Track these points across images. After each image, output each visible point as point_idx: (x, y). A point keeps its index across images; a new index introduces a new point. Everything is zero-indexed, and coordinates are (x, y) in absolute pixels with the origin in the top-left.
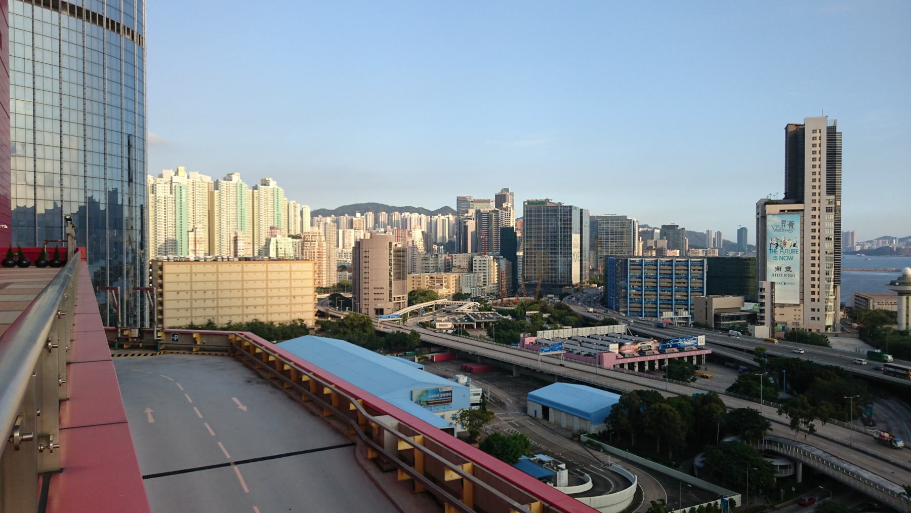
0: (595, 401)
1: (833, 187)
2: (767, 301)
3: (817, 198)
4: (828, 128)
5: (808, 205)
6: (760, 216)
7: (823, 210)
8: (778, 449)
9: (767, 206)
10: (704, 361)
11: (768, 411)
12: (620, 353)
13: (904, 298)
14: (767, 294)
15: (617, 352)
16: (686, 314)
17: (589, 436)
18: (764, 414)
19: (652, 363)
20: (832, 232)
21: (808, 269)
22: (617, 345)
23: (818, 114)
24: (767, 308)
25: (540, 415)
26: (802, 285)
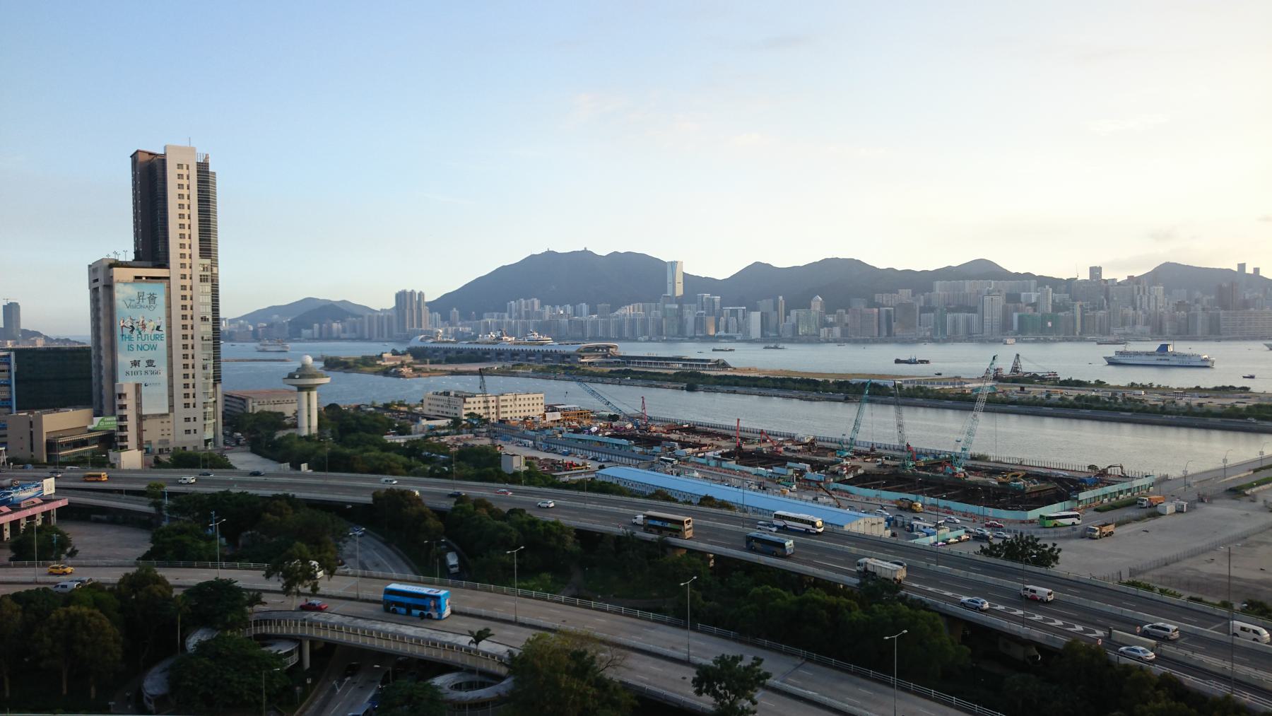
1: (207, 249)
2: (130, 413)
3: (187, 261)
4: (199, 164)
5: (174, 270)
6: (100, 285)
7: (196, 278)
8: (271, 630)
9: (115, 269)
10: (54, 521)
11: (247, 578)
13: (305, 393)
14: (130, 401)
18: (240, 584)
20: (209, 309)
21: (178, 362)
23: (184, 143)
24: (131, 423)
26: (171, 386)
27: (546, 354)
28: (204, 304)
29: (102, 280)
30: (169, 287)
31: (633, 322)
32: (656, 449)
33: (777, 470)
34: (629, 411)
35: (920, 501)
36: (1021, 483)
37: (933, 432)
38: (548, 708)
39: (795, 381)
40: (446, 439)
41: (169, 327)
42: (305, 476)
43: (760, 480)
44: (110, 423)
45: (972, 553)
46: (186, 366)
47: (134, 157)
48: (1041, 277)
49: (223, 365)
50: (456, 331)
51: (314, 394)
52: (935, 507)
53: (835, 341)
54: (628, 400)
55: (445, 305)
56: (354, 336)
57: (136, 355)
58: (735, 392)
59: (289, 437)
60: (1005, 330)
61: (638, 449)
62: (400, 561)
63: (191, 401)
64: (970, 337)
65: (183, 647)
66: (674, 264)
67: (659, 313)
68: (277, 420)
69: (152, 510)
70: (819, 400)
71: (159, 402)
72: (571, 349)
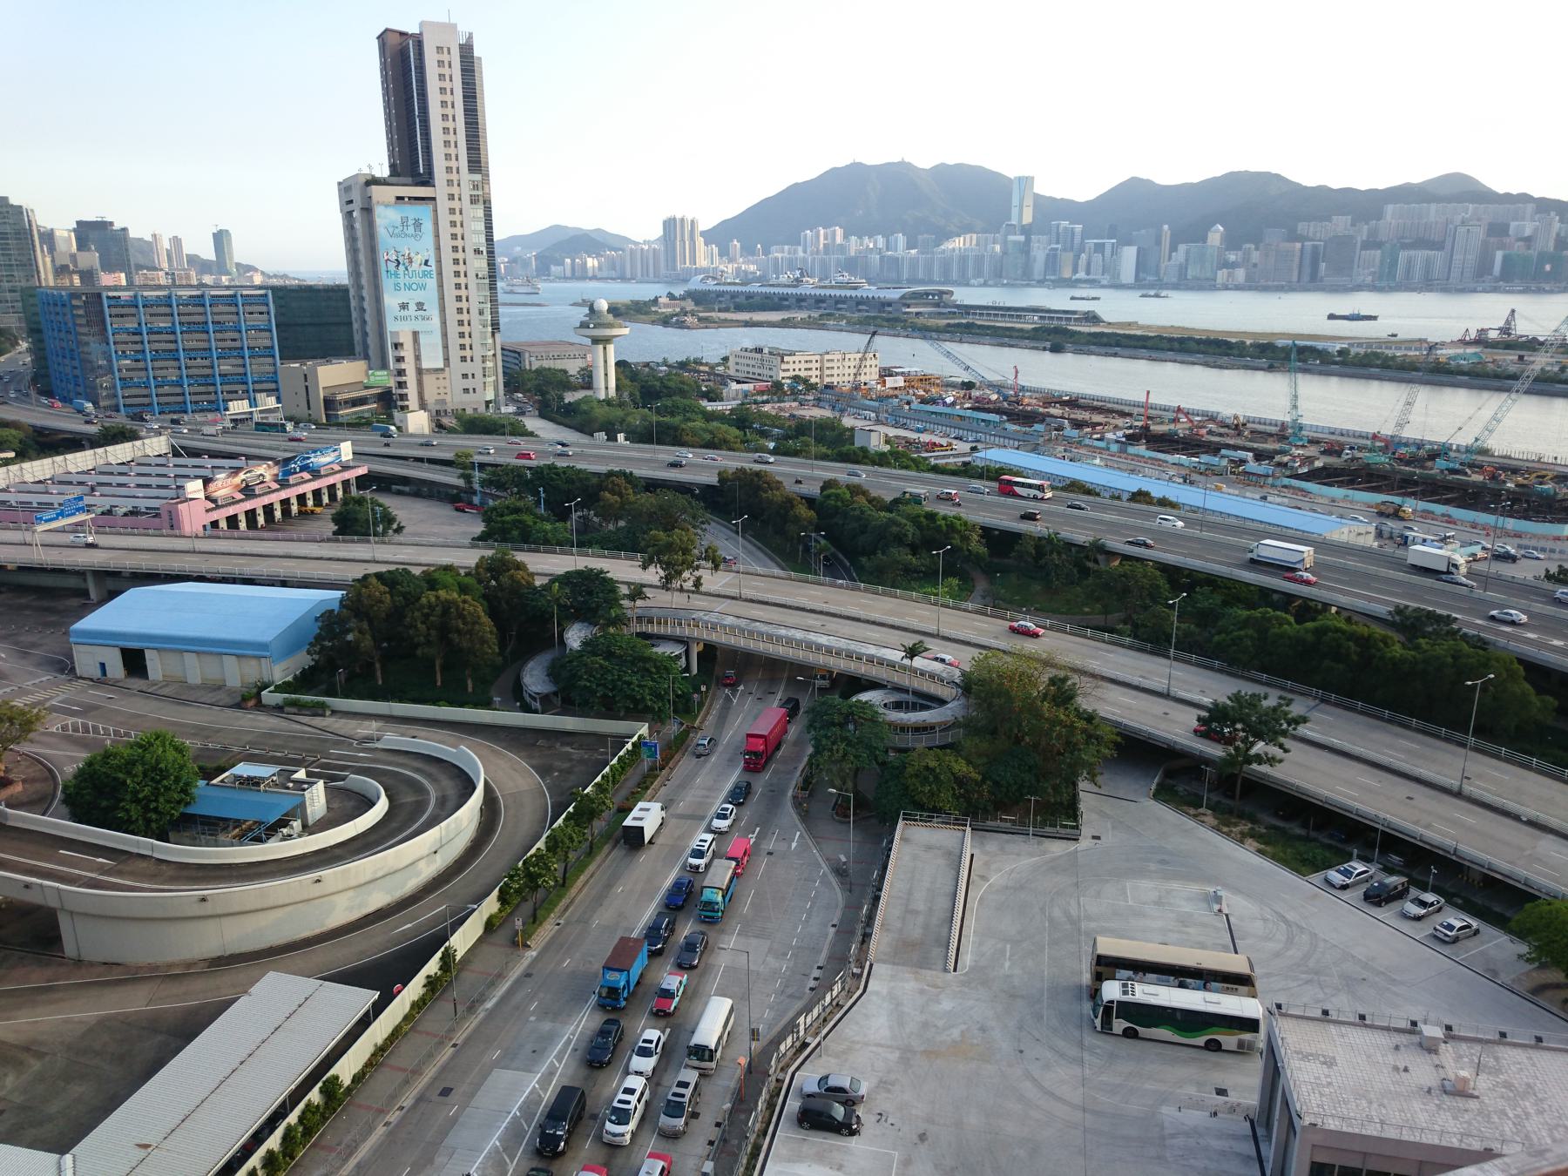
0: (264, 614)
1: (476, 163)
2: (409, 366)
4: (461, 47)
5: (440, 190)
8: (654, 629)
11: (623, 570)
12: (207, 498)
13: (601, 347)
14: (408, 352)
15: (201, 495)
16: (271, 402)
17: (280, 689)
19: (268, 510)
20: (483, 239)
22: (200, 482)
23: (442, 18)
24: (411, 378)
25: (116, 669)
26: (445, 335)
27: (860, 302)
28: (476, 232)
29: (357, 200)
30: (435, 211)
31: (963, 259)
32: (1037, 427)
33: (1205, 458)
34: (992, 377)
35: (1410, 505)
36: (1549, 486)
37: (1446, 419)
38: (1027, 739)
39: (1199, 342)
40: (767, 408)
41: (439, 261)
42: (623, 447)
43: (1183, 472)
44: (383, 379)
45: (1530, 577)
46: (460, 311)
47: (382, 38)
48: (1542, 200)
49: (501, 310)
50: (738, 269)
51: (611, 348)
52: (1427, 514)
53: (1238, 288)
54: (994, 364)
55: (720, 236)
56: (613, 274)
57: (404, 296)
58: (1115, 355)
59: (586, 400)
60: (1482, 278)
61: (1012, 427)
62: (761, 555)
63: (468, 353)
64: (1429, 283)
65: (562, 643)
66: (1026, 182)
67: (998, 248)
68: (562, 381)
69: (461, 483)
70: (1232, 367)
71: (437, 356)
72: (894, 295)
